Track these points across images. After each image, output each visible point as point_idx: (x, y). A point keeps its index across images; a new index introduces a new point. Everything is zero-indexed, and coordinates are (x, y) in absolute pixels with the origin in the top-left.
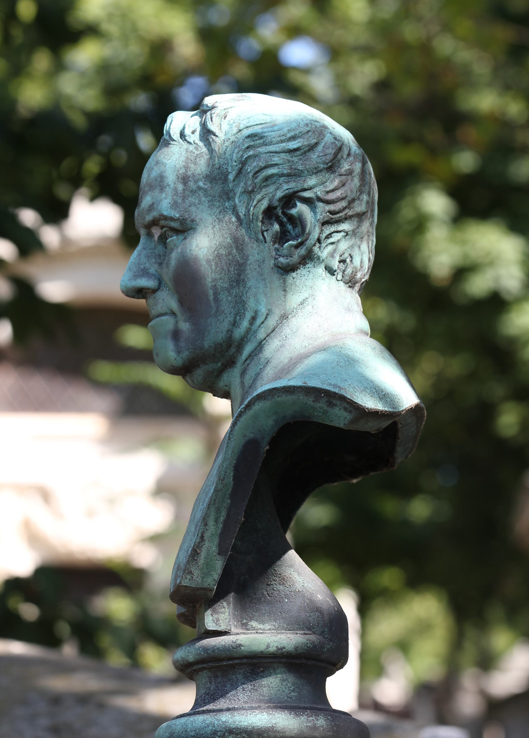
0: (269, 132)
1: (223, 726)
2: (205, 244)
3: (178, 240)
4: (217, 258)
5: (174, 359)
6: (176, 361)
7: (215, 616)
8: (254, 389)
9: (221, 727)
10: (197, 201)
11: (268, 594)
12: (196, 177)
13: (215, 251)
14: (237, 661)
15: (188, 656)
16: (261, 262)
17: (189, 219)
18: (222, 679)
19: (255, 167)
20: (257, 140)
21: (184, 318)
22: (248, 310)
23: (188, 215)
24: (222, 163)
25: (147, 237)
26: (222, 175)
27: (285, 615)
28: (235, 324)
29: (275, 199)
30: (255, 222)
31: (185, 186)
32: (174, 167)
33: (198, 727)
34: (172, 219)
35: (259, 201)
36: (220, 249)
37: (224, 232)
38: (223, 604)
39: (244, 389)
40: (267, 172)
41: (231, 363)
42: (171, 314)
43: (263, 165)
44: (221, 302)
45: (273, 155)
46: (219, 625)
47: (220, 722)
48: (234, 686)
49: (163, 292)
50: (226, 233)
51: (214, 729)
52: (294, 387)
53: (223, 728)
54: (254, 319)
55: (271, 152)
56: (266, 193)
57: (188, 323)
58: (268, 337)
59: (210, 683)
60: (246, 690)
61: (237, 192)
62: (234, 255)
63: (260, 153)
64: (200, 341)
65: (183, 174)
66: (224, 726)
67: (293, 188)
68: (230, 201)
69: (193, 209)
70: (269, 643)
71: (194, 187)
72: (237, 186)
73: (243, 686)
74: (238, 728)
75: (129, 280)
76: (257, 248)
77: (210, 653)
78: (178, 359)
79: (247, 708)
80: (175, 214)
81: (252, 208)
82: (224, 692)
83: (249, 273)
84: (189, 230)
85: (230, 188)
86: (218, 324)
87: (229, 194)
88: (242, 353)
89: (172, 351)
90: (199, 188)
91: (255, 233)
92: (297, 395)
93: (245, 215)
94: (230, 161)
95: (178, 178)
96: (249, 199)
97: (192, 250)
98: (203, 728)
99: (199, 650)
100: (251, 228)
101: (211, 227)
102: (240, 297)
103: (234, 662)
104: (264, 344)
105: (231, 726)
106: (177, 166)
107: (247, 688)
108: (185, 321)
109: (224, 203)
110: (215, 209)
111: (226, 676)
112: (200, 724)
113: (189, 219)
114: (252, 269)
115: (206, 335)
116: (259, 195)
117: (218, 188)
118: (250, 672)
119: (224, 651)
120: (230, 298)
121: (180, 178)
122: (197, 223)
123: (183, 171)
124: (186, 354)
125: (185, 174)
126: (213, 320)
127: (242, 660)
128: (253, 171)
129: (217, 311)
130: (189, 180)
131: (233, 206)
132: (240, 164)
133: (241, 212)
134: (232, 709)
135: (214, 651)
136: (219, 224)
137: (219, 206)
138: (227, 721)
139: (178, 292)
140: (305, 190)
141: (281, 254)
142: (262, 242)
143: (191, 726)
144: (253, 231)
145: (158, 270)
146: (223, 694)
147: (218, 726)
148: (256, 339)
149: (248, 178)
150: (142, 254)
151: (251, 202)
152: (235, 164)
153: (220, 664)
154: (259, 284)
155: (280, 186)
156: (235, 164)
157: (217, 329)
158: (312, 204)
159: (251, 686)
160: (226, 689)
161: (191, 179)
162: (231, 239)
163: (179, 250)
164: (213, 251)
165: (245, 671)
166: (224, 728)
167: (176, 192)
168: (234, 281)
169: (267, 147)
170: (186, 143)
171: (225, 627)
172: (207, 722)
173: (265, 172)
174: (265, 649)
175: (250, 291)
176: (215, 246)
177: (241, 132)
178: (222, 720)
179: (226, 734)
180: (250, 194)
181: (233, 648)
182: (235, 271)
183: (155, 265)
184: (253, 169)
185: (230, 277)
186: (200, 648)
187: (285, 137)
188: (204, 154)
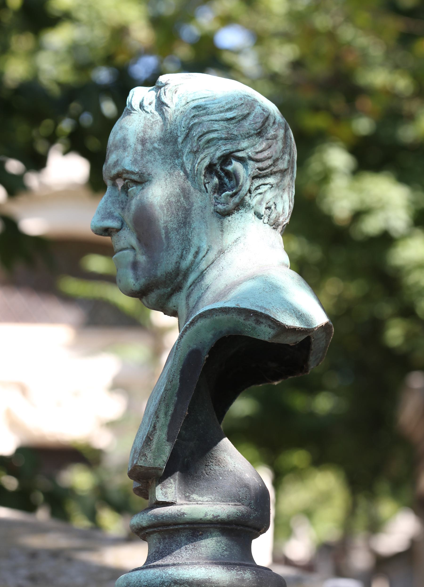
0: (211, 104)
2: (159, 193)
3: (137, 189)
4: (168, 205)
6: (134, 286)
7: (164, 490)
9: (168, 579)
10: (153, 158)
11: (206, 473)
12: (152, 140)
13: (167, 198)
15: (142, 522)
17: (146, 173)
19: (199, 132)
20: (201, 110)
21: (141, 252)
23: (145, 170)
24: (173, 129)
25: (112, 187)
31: (143, 146)
33: (149, 579)
34: (132, 173)
36: (170, 197)
38: (170, 480)
39: (188, 309)
40: (209, 136)
41: (178, 288)
42: (130, 248)
43: (205, 131)
45: (213, 123)
46: (167, 497)
47: (167, 575)
48: (179, 546)
49: (125, 231)
50: (175, 184)
51: (162, 580)
52: (229, 308)
53: (169, 580)
55: (212, 121)
56: (208, 153)
57: (144, 256)
58: (208, 268)
60: (188, 549)
61: (184, 152)
62: (182, 202)
63: (203, 121)
64: (154, 271)
65: (142, 137)
66: (170, 578)
68: (179, 159)
69: (150, 165)
71: (151, 148)
73: (186, 546)
74: (181, 580)
78: (136, 284)
79: (189, 564)
80: (135, 169)
81: (196, 165)
83: (194, 217)
84: (146, 182)
86: (168, 257)
87: (178, 154)
88: (188, 281)
89: (131, 279)
90: (155, 148)
93: (191, 170)
94: (179, 127)
95: (138, 140)
96: (194, 157)
99: (151, 517)
100: (196, 181)
101: (163, 179)
102: (187, 236)
103: (179, 527)
104: (205, 274)
105: (176, 578)
106: (137, 130)
107: (188, 548)
108: (143, 254)
110: (167, 165)
113: (146, 173)
114: (196, 214)
115: (159, 266)
116: (202, 155)
117: (169, 149)
118: (191, 535)
119: (171, 518)
120: (178, 237)
121: (139, 140)
123: (141, 134)
124: (142, 281)
126: (164, 254)
127: (185, 526)
129: (168, 247)
130: (146, 142)
131: (181, 163)
133: (188, 168)
134: (177, 564)
135: (162, 518)
137: (171, 163)
138: (172, 574)
140: (239, 151)
142: (204, 192)
144: (197, 183)
145: (121, 213)
147: (166, 578)
148: (199, 269)
149: (193, 141)
150: (109, 201)
151: (196, 160)
152: (183, 129)
153: (167, 528)
155: (219, 148)
156: (183, 129)
157: (167, 261)
158: (245, 162)
159: (192, 546)
161: (148, 141)
162: (179, 190)
163: (138, 198)
165: (188, 534)
167: (136, 151)
168: (182, 223)
169: (209, 116)
171: (172, 499)
173: (207, 137)
175: (195, 231)
176: (167, 195)
177: (188, 104)
178: (168, 573)
181: (178, 516)
183: (118, 209)
185: (178, 220)
187: (224, 108)
188: (158, 121)
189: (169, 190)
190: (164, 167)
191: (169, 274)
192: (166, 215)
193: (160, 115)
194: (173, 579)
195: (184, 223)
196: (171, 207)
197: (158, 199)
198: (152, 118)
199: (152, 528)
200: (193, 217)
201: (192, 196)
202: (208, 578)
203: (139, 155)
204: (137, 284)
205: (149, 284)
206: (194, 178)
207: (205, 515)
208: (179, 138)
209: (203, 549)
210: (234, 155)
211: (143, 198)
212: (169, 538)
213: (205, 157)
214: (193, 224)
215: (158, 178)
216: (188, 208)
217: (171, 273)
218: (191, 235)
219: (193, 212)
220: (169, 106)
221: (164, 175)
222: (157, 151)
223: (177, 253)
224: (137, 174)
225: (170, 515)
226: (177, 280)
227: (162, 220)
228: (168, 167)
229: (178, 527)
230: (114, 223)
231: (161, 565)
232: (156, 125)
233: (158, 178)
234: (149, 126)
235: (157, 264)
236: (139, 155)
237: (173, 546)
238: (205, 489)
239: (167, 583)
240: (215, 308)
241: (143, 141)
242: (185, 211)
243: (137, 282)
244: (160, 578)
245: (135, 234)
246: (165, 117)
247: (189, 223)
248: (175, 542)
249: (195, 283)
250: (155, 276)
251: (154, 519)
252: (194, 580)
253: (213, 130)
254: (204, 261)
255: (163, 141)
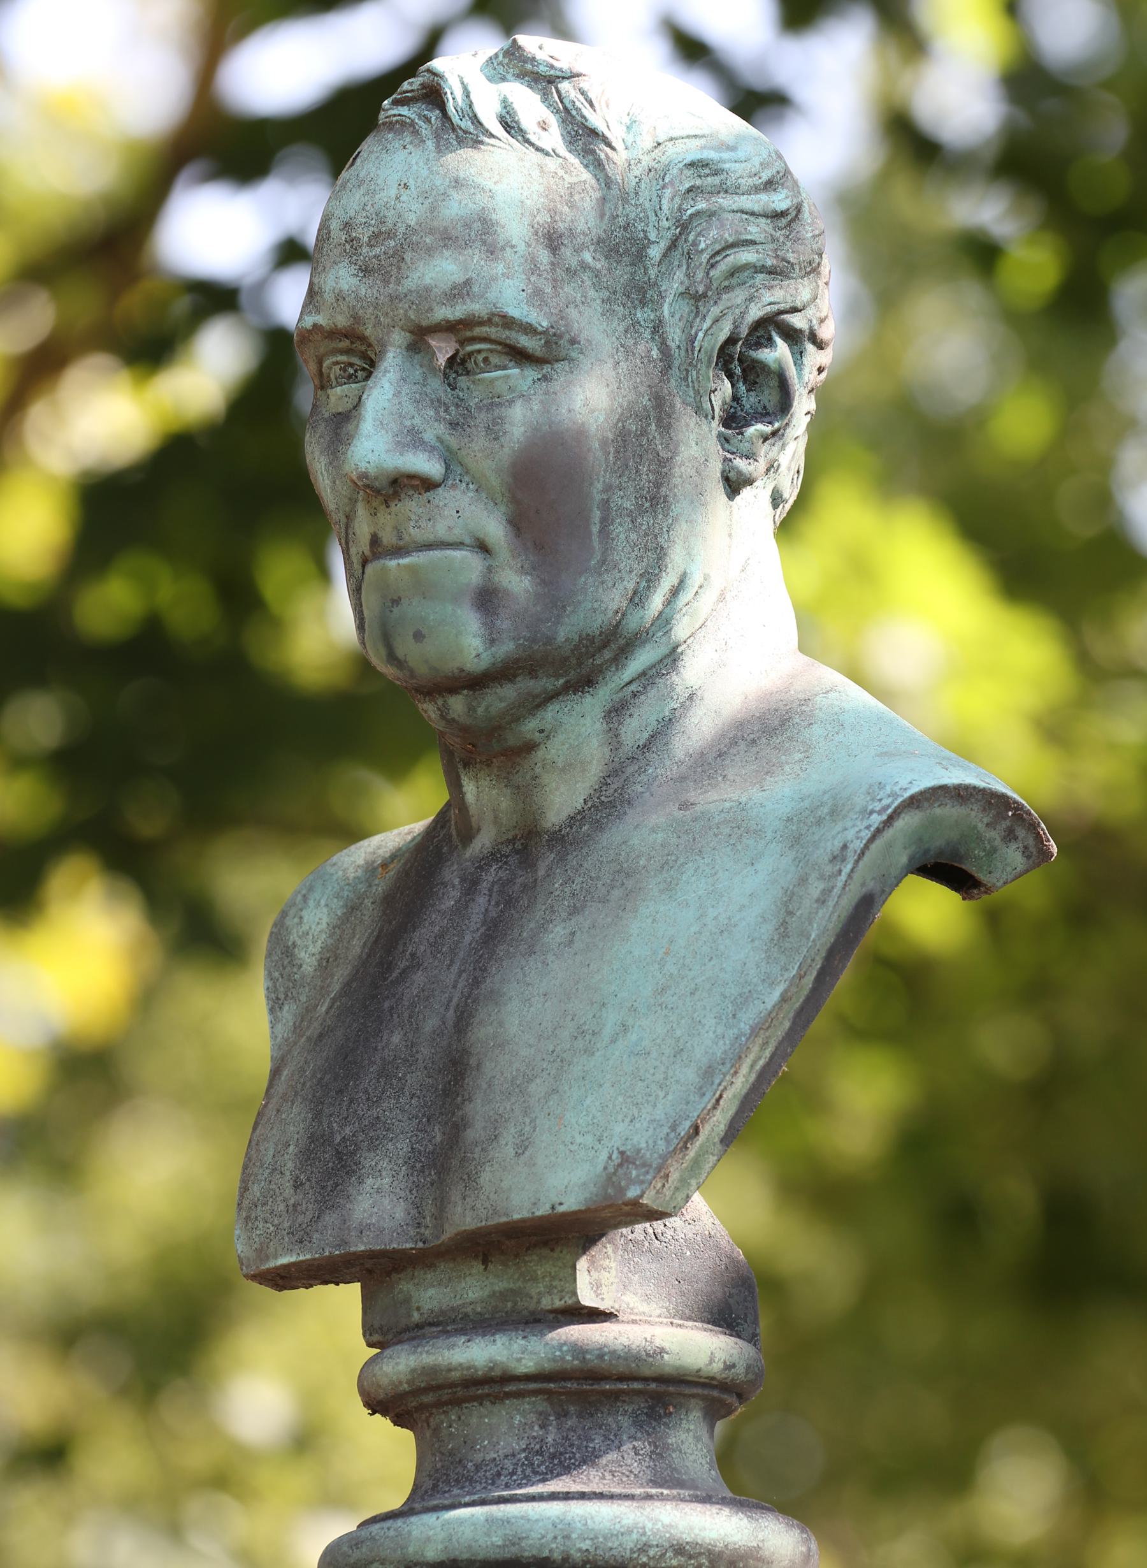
0: (730, 161)
1: (665, 1536)
2: (602, 402)
3: (524, 378)
4: (619, 439)
5: (474, 655)
6: (476, 660)
7: (595, 1274)
8: (666, 756)
9: (661, 1537)
10: (579, 295)
11: (655, 1234)
12: (578, 239)
13: (619, 420)
14: (637, 1386)
15: (519, 1360)
16: (701, 462)
17: (567, 337)
18: (580, 1422)
19: (715, 241)
21: (519, 565)
22: (668, 570)
23: (565, 326)
24: (632, 216)
26: (631, 243)
27: (686, 1287)
28: (638, 599)
29: (746, 322)
30: (704, 368)
31: (554, 255)
32: (520, 204)
33: (602, 1533)
34: (528, 329)
35: (716, 321)
36: (628, 418)
37: (638, 380)
38: (606, 1248)
41: (585, 683)
42: (472, 546)
43: (731, 240)
44: (615, 543)
45: (746, 219)
46: (601, 1296)
47: (659, 1526)
48: (613, 1441)
49: (458, 492)
50: (641, 382)
51: (644, 1539)
52: (975, 788)
53: (665, 1541)
54: (675, 592)
55: (743, 212)
56: (729, 304)
58: (692, 638)
59: (542, 1427)
60: (641, 1452)
61: (666, 291)
62: (651, 437)
65: (546, 226)
66: (668, 1535)
67: (779, 303)
68: (646, 309)
69: (572, 312)
70: (714, 1351)
71: (573, 262)
72: (670, 273)
73: (634, 1443)
74: (697, 1544)
75: (388, 451)
76: (696, 430)
77: (590, 1359)
78: (484, 656)
79: (688, 1498)
80: (540, 318)
81: (701, 335)
82: (588, 1452)
83: (678, 485)
84: (557, 361)
85: (649, 279)
86: (601, 590)
90: (584, 266)
91: (697, 392)
92: (971, 806)
93: (679, 347)
94: (651, 214)
96: (692, 311)
97: (574, 411)
98: (617, 1535)
99: (560, 1350)
100: (690, 380)
101: (610, 364)
104: (682, 653)
105: (684, 1536)
106: (528, 202)
107: (642, 1449)
108: (523, 571)
109: (633, 312)
110: (616, 322)
111: (592, 1415)
112: (608, 1524)
113: (567, 337)
114: (684, 477)
117: (622, 273)
118: (646, 1414)
119: (626, 1359)
120: (634, 536)
121: (540, 234)
122: (581, 349)
123: (543, 218)
124: (506, 648)
125: (551, 226)
126: (591, 580)
127: (648, 1385)
128: (710, 250)
129: (603, 561)
130: (562, 243)
132: (677, 227)
134: (658, 1496)
135: (601, 1356)
136: (627, 359)
137: (624, 317)
138: (673, 1524)
139: (514, 500)
140: (795, 310)
141: (735, 451)
142: (706, 417)
143: (583, 1528)
144: (694, 387)
146: (589, 1458)
147: (654, 1534)
148: (670, 637)
149: (698, 264)
150: (404, 393)
151: (698, 320)
152: (666, 224)
153: (595, 1387)
154: (695, 514)
155: (756, 294)
156: (666, 224)
157: (596, 603)
159: (650, 1445)
160: (591, 1445)
161: (566, 242)
162: (650, 400)
164: (615, 421)
165: (638, 1410)
166: (669, 1540)
167: (535, 265)
168: (646, 498)
170: (533, 150)
172: (625, 1522)
173: (732, 257)
174: (707, 1365)
175: (677, 527)
176: (619, 411)
177: (660, 148)
178: (662, 1521)
179: (668, 1555)
180: (698, 300)
181: (648, 1355)
182: (650, 474)
183: (436, 424)
184: (711, 244)
185: (638, 487)
186: (561, 1345)
187: (760, 178)
189: (625, 397)
190: (607, 325)
191: (588, 640)
192: (611, 469)
193: (586, 166)
194: (674, 1539)
195: (652, 499)
196: (625, 446)
197: (598, 417)
198: (566, 172)
199: (535, 1382)
200: (675, 486)
201: (677, 424)
202: (756, 1545)
203: (545, 279)
204: (488, 656)
205: (517, 660)
206: (684, 373)
207: (711, 1360)
208: (651, 246)
209: (674, 1456)
210: (783, 320)
211: (555, 408)
212: (580, 1416)
213: (721, 317)
214: (673, 507)
215: (596, 355)
216: (665, 456)
217: (594, 637)
218: (666, 537)
219: (676, 471)
220: (613, 144)
221: (610, 349)
222: (590, 274)
223: (625, 583)
224: (542, 336)
225: (626, 1350)
226: (593, 660)
227: (601, 481)
228: (618, 328)
229: (628, 1385)
230: (433, 465)
231: (607, 1496)
232: (582, 195)
233: (596, 355)
234: (562, 197)
235: (564, 607)
236: (545, 279)
237: (593, 1440)
238: (653, 1281)
239: (657, 1549)
240: (946, 785)
241: (553, 240)
242: (656, 465)
243: (490, 649)
244: (638, 1532)
245: (503, 508)
246: (608, 177)
247: (664, 502)
248: (600, 1428)
249: (647, 677)
250: (549, 640)
251: (569, 1358)
252: (727, 1549)
253: (747, 240)
254: (686, 617)
255: (606, 249)
